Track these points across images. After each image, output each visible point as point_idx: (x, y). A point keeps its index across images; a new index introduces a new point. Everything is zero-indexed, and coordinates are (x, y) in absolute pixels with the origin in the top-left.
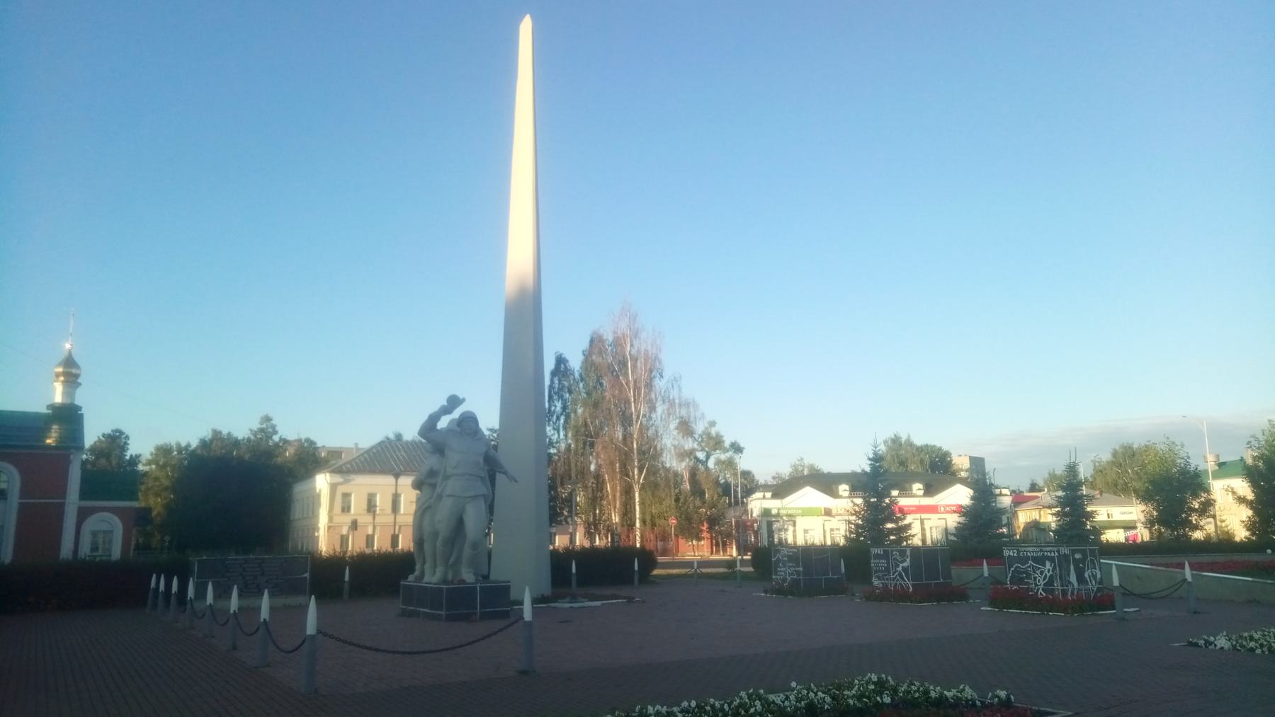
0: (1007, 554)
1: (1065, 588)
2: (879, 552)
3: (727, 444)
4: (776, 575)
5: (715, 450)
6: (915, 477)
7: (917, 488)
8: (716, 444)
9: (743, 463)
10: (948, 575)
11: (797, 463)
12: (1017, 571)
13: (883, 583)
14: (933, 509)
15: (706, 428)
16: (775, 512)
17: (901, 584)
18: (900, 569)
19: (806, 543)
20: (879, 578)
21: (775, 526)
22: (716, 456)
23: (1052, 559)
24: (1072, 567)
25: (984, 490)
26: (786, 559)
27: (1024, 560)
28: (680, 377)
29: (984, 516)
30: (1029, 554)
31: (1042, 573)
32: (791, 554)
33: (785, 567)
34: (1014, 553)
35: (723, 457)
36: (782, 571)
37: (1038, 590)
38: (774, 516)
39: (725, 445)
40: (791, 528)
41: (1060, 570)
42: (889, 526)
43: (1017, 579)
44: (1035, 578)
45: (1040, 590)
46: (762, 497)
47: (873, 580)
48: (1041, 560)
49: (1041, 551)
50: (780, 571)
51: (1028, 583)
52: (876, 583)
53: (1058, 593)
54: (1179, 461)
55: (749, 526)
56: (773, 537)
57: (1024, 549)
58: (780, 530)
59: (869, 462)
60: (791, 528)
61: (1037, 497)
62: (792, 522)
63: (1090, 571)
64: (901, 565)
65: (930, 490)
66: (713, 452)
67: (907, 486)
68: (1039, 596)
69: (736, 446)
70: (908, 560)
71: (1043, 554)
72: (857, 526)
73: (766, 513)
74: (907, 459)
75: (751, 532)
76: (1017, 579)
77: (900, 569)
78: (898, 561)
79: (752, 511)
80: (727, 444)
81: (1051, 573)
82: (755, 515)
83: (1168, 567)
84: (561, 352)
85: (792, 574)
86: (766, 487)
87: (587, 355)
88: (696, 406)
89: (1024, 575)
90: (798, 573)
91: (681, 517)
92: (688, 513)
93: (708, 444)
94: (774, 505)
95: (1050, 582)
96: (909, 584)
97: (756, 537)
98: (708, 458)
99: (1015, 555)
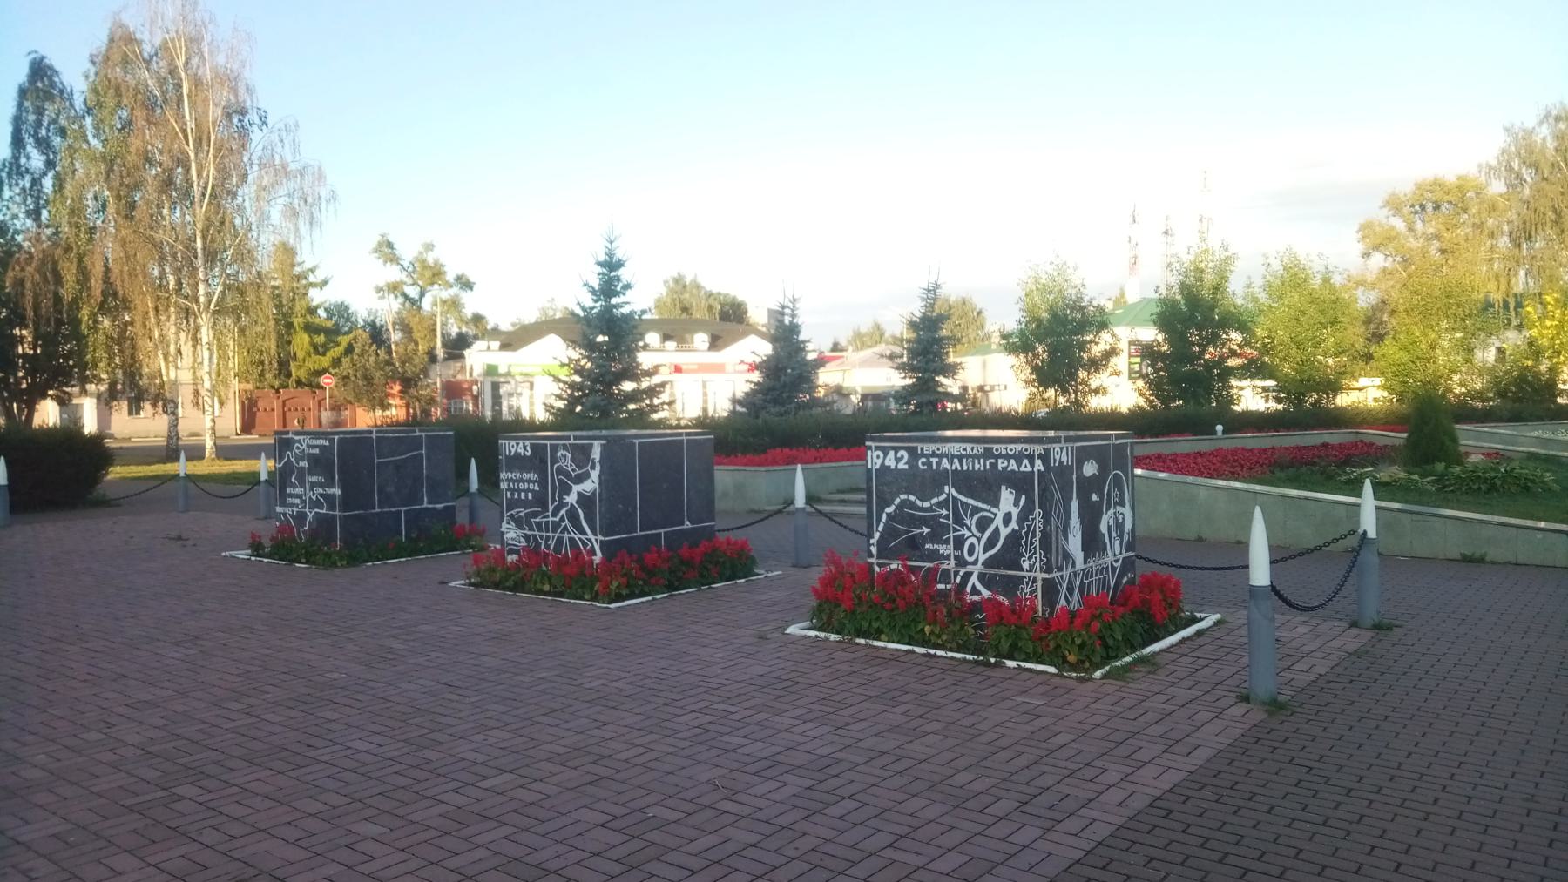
0: (879, 462)
1: (1054, 575)
2: (521, 451)
3: (450, 277)
4: (284, 504)
5: (432, 284)
6: (699, 325)
7: (701, 339)
8: (434, 275)
9: (472, 304)
10: (706, 504)
11: (548, 305)
12: (905, 516)
13: (527, 538)
14: (719, 368)
15: (421, 253)
16: (502, 370)
17: (572, 540)
18: (572, 498)
19: (705, 410)
20: (519, 523)
21: (502, 391)
22: (433, 293)
23: (1020, 484)
24: (1075, 505)
25: (785, 335)
26: (304, 464)
27: (931, 482)
28: (297, 126)
29: (789, 371)
30: (945, 463)
31: (983, 524)
32: (317, 451)
33: (302, 484)
34: (898, 460)
35: (446, 294)
36: (298, 496)
37: (968, 575)
38: (501, 375)
39: (447, 279)
40: (526, 392)
41: (1047, 520)
42: (628, 386)
43: (903, 542)
44: (959, 542)
45: (974, 579)
46: (485, 348)
47: (504, 525)
48: (984, 486)
49: (988, 454)
50: (291, 496)
51: (934, 556)
52: (512, 534)
53: (1032, 594)
54: (1069, 291)
55: (466, 389)
56: (500, 405)
57: (933, 447)
58: (511, 395)
59: (599, 269)
60: (526, 392)
61: (842, 357)
62: (528, 384)
63: (1112, 511)
64: (576, 488)
65: (716, 343)
66: (429, 288)
67: (688, 336)
68: (969, 599)
69: (464, 280)
70: (595, 474)
71: (994, 466)
72: (572, 386)
73: (491, 371)
74: (691, 306)
75: (469, 398)
76: (903, 542)
77: (572, 498)
78: (568, 475)
79: (472, 369)
80: (450, 277)
81: (1014, 525)
82: (475, 374)
83: (1180, 471)
84: (43, 52)
85: (317, 504)
86: (495, 333)
87: (103, 61)
88: (320, 177)
89: (926, 530)
90: (329, 499)
91: (356, 376)
92: (367, 370)
93: (422, 276)
94: (504, 360)
95: (1010, 554)
96: (594, 541)
97: (476, 405)
98: (422, 295)
99: (902, 466)
